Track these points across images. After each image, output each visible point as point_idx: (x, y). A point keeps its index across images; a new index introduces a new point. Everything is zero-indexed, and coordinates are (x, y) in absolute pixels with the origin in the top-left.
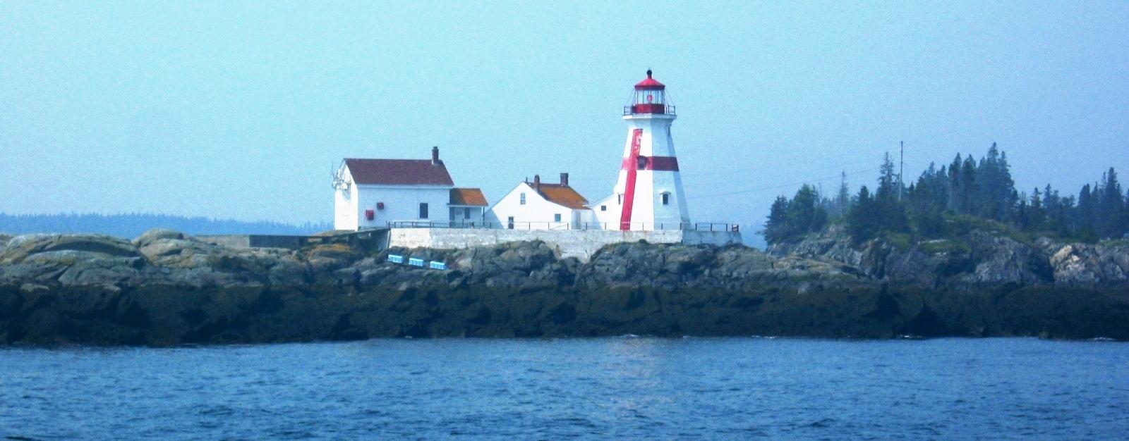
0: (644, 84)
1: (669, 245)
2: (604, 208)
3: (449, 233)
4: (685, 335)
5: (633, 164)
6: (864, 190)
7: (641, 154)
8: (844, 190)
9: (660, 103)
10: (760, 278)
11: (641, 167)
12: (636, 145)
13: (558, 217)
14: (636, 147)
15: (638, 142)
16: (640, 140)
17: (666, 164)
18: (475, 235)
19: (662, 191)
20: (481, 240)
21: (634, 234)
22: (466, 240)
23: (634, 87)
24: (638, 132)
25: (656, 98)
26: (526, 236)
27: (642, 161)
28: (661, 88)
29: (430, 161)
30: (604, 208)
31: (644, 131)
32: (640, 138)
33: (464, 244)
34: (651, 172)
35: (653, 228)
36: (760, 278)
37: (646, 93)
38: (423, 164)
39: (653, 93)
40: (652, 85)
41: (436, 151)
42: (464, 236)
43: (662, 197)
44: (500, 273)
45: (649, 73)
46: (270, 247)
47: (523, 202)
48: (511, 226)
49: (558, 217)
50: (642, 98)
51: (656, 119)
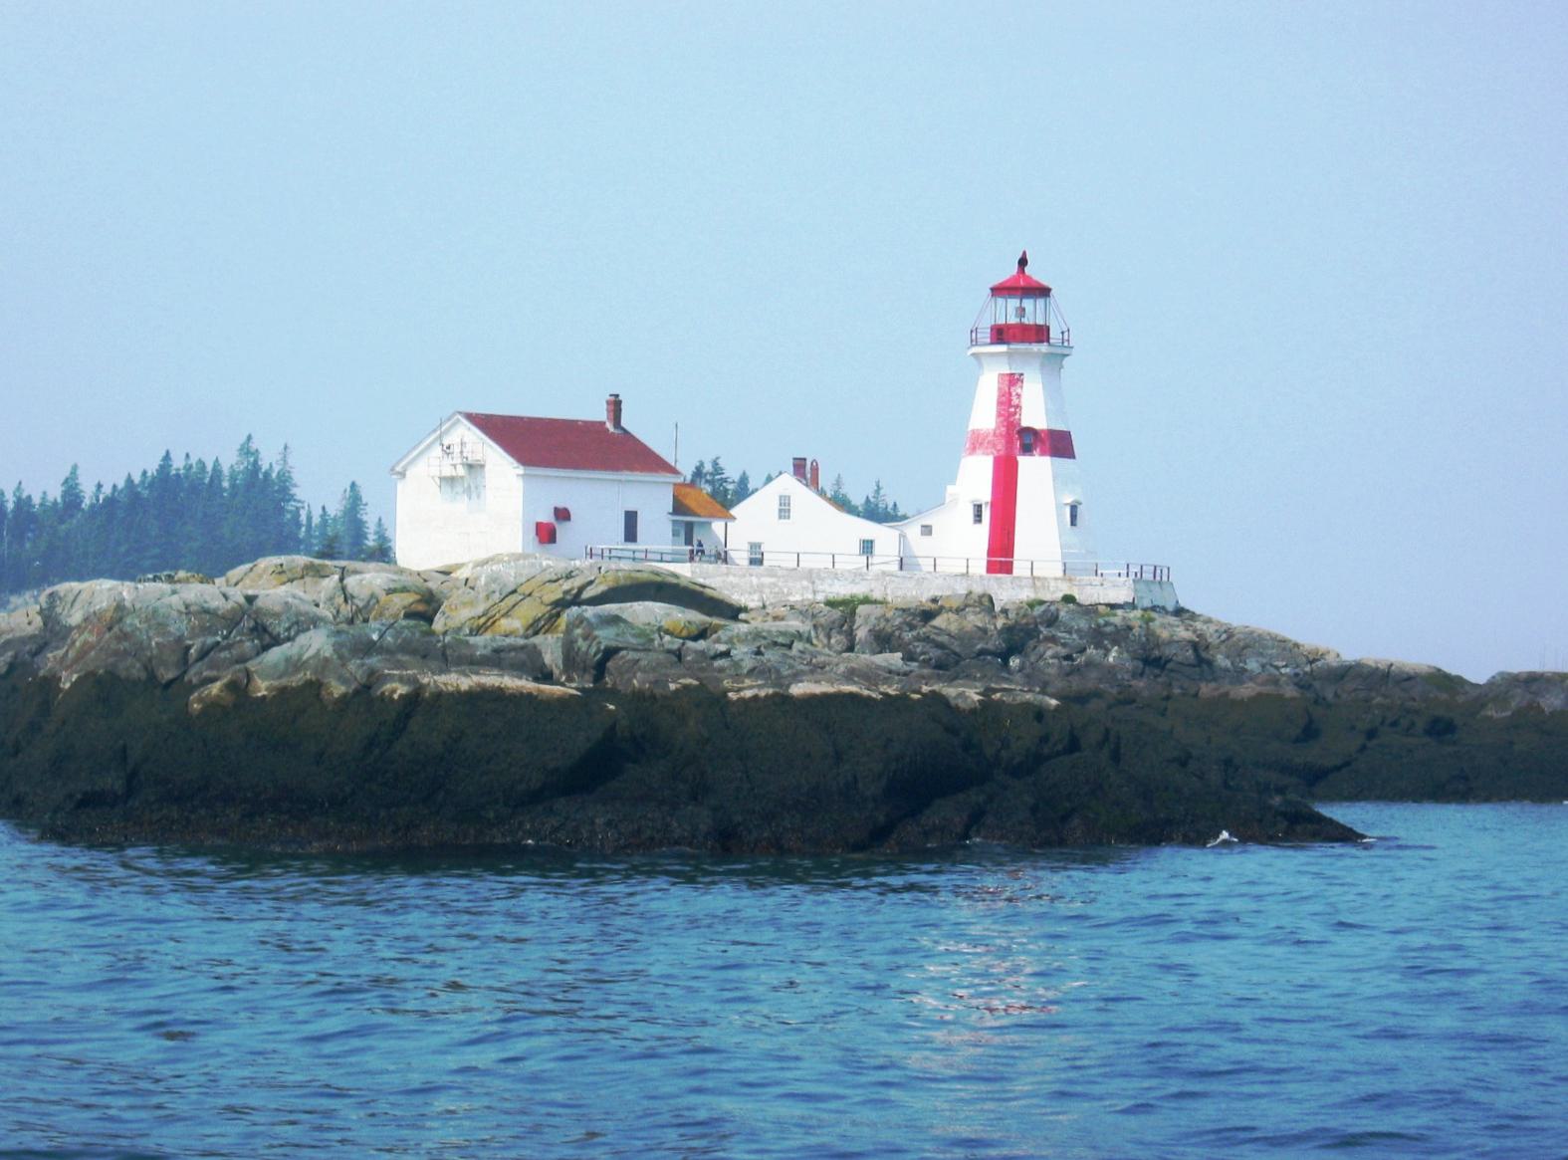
0: (1008, 285)
1: (1113, 606)
2: (927, 530)
3: (727, 574)
4: (264, 697)
5: (1009, 442)
6: (115, 486)
7: (1025, 423)
8: (295, 486)
9: (1040, 322)
10: (1342, 677)
11: (1027, 450)
12: (1008, 405)
13: (867, 547)
14: (1012, 410)
15: (1015, 401)
16: (1019, 396)
17: (1059, 444)
18: (773, 580)
19: (1069, 500)
20: (785, 590)
21: (1052, 584)
22: (760, 589)
23: (989, 291)
24: (1013, 380)
25: (1034, 312)
26: (864, 583)
27: (1029, 440)
28: (1043, 292)
29: (603, 424)
30: (927, 530)
31: (1026, 378)
32: (1019, 391)
33: (756, 597)
34: (1047, 460)
35: (985, 569)
36: (1342, 677)
37: (1013, 303)
38: (593, 429)
39: (1028, 304)
40: (1024, 287)
41: (615, 406)
42: (755, 580)
43: (1068, 510)
44: (957, 663)
45: (1023, 262)
46: (123, 576)
47: (784, 511)
48: (757, 561)
49: (867, 547)
50: (1007, 311)
51: (1052, 354)
